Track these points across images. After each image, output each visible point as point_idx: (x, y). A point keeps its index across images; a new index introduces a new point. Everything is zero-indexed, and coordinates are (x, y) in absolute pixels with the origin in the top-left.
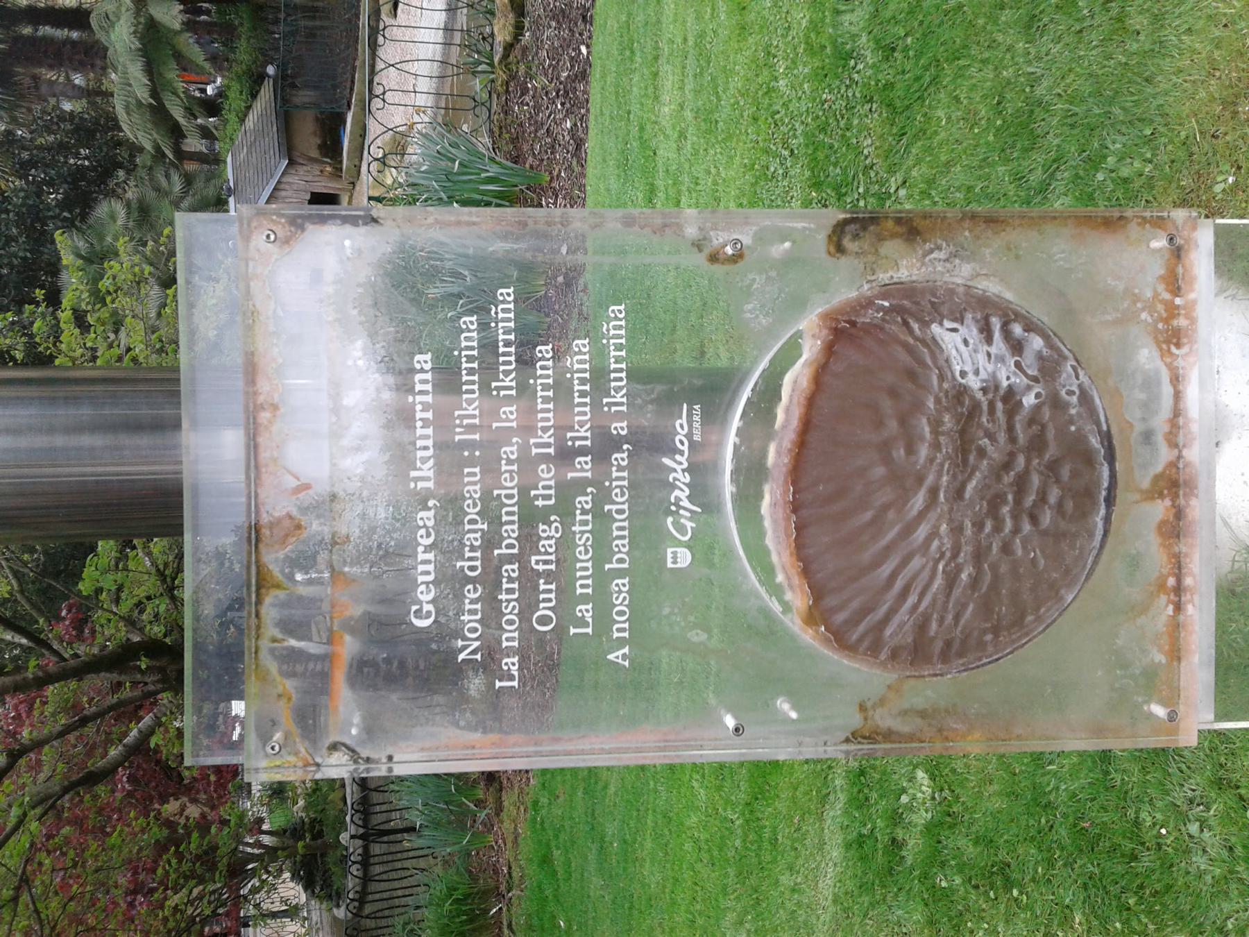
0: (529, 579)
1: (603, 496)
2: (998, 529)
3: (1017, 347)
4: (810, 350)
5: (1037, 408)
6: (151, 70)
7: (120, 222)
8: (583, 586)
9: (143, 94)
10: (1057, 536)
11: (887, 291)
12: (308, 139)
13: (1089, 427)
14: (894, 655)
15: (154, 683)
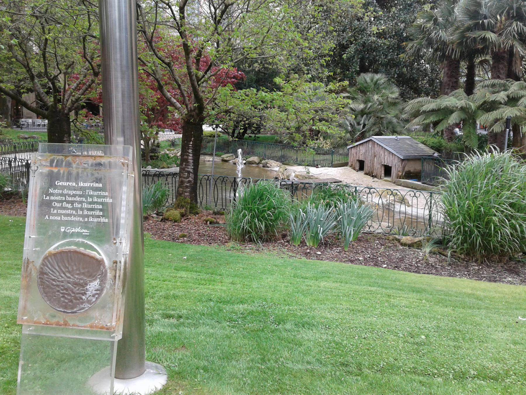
0: (62, 202)
1: (75, 216)
2: (62, 290)
3: (94, 296)
4: (98, 256)
5: (82, 299)
6: (433, 111)
7: (390, 95)
8: (60, 211)
9: (424, 108)
10: (59, 301)
11: (106, 271)
12: (412, 167)
13: (78, 309)
14: (42, 268)
15: (190, 107)
